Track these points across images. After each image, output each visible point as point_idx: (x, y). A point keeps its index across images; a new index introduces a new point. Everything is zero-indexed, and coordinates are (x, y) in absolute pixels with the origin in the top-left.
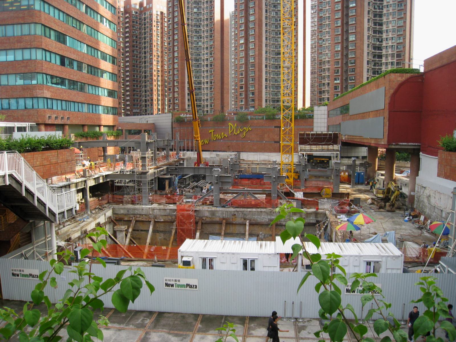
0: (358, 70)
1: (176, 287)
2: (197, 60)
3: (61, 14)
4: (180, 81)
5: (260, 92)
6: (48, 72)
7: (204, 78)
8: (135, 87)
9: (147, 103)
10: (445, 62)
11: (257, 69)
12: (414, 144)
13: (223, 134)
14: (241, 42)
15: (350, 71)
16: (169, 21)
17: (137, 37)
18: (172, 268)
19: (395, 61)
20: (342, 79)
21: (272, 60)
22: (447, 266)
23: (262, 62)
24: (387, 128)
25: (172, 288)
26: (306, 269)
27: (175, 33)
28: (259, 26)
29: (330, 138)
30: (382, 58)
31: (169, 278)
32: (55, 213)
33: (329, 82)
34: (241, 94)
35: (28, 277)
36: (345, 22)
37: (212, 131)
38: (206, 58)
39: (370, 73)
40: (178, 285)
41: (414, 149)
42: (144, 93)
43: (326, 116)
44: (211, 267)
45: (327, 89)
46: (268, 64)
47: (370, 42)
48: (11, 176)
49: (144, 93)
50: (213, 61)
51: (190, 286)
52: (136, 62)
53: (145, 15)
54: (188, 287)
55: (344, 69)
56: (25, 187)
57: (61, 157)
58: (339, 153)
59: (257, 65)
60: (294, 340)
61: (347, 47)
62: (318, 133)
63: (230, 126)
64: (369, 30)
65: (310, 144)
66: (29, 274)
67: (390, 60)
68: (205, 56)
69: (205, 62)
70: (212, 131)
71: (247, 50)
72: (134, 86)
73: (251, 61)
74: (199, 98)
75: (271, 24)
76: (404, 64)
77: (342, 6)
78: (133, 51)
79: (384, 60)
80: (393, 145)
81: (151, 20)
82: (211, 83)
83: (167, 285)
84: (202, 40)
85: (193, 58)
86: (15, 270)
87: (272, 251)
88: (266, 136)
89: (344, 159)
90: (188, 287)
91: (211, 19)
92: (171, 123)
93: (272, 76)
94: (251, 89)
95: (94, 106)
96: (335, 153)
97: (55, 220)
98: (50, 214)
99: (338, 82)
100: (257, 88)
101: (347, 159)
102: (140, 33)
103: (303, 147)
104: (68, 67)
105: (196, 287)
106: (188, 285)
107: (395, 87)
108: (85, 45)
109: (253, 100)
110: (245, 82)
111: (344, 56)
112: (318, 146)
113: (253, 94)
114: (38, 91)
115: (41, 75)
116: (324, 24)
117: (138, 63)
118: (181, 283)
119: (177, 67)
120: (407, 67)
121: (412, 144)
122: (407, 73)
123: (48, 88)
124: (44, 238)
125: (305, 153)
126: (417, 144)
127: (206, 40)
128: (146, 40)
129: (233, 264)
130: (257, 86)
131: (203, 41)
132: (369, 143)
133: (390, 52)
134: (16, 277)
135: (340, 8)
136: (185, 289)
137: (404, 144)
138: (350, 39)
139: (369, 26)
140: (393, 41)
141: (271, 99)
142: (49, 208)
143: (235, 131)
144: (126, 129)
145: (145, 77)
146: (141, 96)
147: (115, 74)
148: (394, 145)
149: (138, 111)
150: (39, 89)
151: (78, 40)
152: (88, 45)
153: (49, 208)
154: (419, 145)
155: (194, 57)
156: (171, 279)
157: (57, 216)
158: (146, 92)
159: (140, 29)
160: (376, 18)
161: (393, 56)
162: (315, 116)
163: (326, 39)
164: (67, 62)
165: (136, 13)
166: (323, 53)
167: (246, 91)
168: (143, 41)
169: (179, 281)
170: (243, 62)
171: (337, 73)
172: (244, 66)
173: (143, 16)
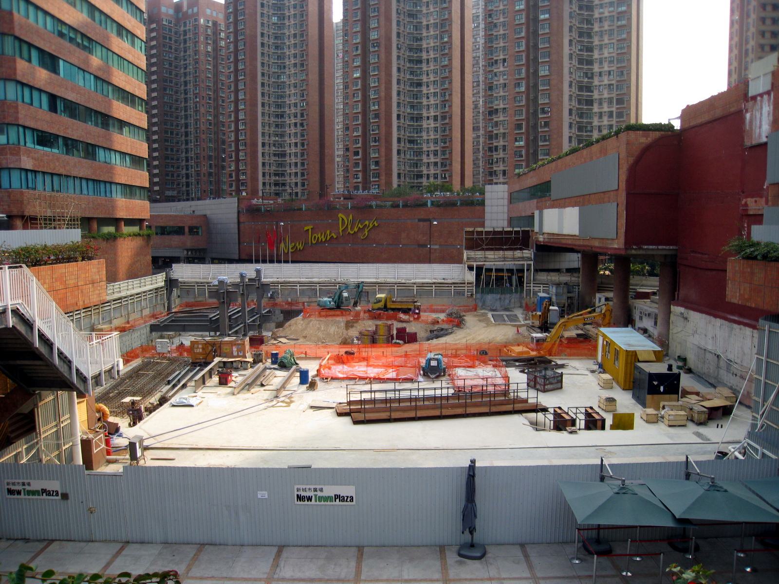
1: (316, 501)
2: (279, 106)
3: (49, 19)
4: (248, 141)
5: (389, 161)
6: (27, 124)
7: (290, 137)
8: (169, 153)
10: (719, 113)
11: (383, 122)
13: (328, 232)
14: (355, 75)
15: (541, 126)
16: (228, 38)
17: (170, 65)
19: (614, 109)
20: (527, 139)
22: (761, 446)
23: (391, 110)
24: (623, 221)
25: (309, 503)
28: (386, 48)
29: (517, 239)
30: (592, 105)
31: (304, 487)
32: (85, 377)
33: (506, 144)
34: (357, 165)
35: (39, 495)
36: (531, 44)
37: (310, 227)
38: (293, 102)
39: (573, 129)
40: (319, 497)
41: (665, 256)
42: (184, 163)
43: (506, 202)
45: (501, 155)
46: (401, 113)
47: (574, 77)
48: (16, 312)
49: (184, 162)
51: (342, 499)
52: (170, 108)
53: (185, 26)
54: (337, 500)
55: (531, 123)
56: (38, 330)
57: (83, 276)
58: (532, 263)
59: (382, 115)
60: (531, 581)
61: (536, 86)
62: (496, 230)
63: (341, 219)
64: (571, 58)
65: (483, 249)
66: (40, 489)
67: (606, 108)
68: (292, 98)
69: (292, 108)
70: (310, 227)
72: (167, 149)
73: (372, 108)
76: (629, 115)
77: (527, 18)
78: (165, 89)
79: (596, 108)
81: (196, 34)
82: (303, 145)
83: (300, 498)
86: (14, 484)
88: (404, 235)
89: (539, 273)
90: (337, 500)
91: (302, 35)
92: (236, 215)
94: (373, 155)
95: (108, 185)
96: (525, 263)
100: (383, 154)
101: (545, 274)
102: (176, 58)
103: (472, 253)
104: (63, 114)
106: (337, 497)
108: (92, 77)
109: (378, 175)
110: (362, 144)
111: (531, 101)
112: (497, 252)
113: (377, 163)
114: (8, 156)
115: (15, 128)
116: (497, 48)
117: (173, 110)
118: (325, 493)
119: (243, 117)
120: (633, 121)
121: (664, 247)
123: (29, 152)
124: (54, 424)
125: (475, 264)
126: (671, 247)
127: (293, 72)
128: (188, 70)
130: (383, 150)
131: (288, 73)
132: (588, 246)
133: (606, 95)
134: (16, 496)
135: (523, 21)
136: (331, 503)
137: (651, 247)
138: (541, 73)
139: (572, 52)
140: (611, 77)
143: (349, 227)
144: (158, 224)
145: (187, 134)
146: (178, 168)
148: (635, 249)
149: (175, 193)
150: (12, 154)
151: (79, 68)
152: (96, 77)
154: (675, 249)
156: (308, 487)
158: (187, 161)
159: (176, 51)
160: (582, 39)
161: (610, 101)
162: (487, 202)
163: (500, 72)
164: (60, 106)
165: (170, 22)
166: (495, 95)
168: (182, 71)
169: (321, 490)
170: (359, 110)
173: (182, 29)
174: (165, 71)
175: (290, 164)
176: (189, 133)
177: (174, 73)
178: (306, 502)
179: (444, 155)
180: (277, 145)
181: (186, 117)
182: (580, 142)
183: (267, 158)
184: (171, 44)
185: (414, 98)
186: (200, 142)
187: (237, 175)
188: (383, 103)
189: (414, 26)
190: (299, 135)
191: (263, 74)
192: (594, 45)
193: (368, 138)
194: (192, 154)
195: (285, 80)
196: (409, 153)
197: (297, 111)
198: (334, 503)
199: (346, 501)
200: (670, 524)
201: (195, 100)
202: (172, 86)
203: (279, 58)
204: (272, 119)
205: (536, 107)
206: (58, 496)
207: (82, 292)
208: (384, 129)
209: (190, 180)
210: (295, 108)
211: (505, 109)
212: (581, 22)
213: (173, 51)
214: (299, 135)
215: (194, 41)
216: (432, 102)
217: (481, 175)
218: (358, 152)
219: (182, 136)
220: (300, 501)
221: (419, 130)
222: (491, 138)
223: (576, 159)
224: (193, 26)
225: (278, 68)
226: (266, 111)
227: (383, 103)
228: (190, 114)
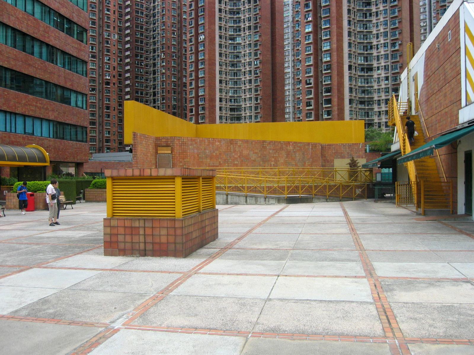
4: (207, 97)
11: (335, 73)
14: (307, 31)
17: (142, 35)
21: (359, 15)
23: (343, 60)
27: (200, 49)
34: (308, 104)
46: (352, 64)
50: (259, 65)
68: (247, 76)
71: (317, 43)
72: (137, 92)
73: (324, 60)
74: (237, 115)
75: (356, 32)
84: (242, 33)
85: (228, 62)
93: (360, 84)
145: (155, 95)
155: (229, 77)
172: (312, 68)
174: (137, 63)
175: (245, 117)
176: (157, 93)
177: (144, 56)
180: (233, 101)
183: (224, 112)
184: (143, 10)
185: (364, 49)
188: (335, 54)
189: (364, 57)
190: (253, 91)
191: (220, 37)
193: (320, 89)
194: (159, 45)
195: (240, 42)
196: (359, 36)
201: (162, 64)
203: (235, 74)
204: (229, 77)
208: (336, 79)
213: (144, 16)
214: (253, 91)
215: (162, 36)
216: (383, 53)
219: (150, 96)
224: (161, 8)
225: (234, 32)
226: (223, 70)
227: (335, 54)
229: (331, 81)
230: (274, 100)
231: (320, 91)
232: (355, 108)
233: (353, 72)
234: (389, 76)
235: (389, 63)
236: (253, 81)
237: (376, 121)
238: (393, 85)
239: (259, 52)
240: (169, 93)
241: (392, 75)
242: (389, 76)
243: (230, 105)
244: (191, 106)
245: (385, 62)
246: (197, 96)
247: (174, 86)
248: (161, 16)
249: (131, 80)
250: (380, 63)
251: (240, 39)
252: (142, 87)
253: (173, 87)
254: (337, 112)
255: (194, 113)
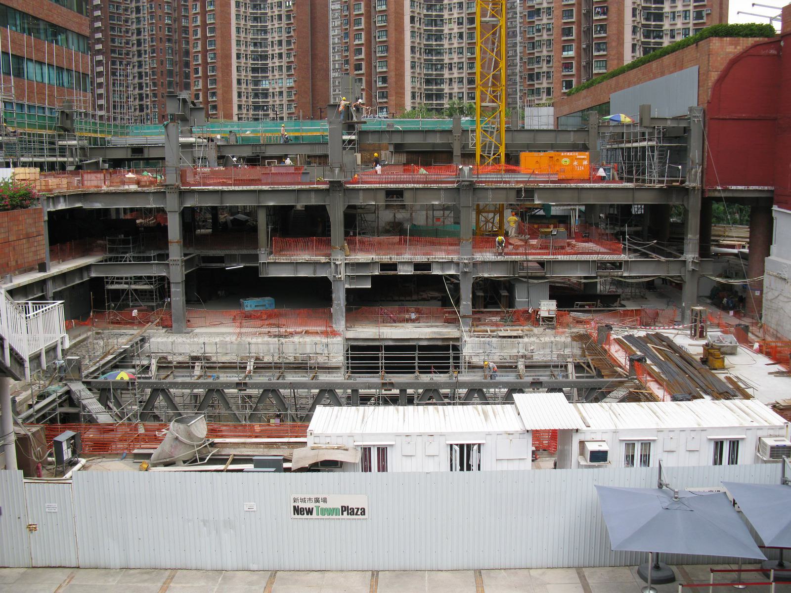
0: (612, 29)
5: (400, 76)
9: (144, 102)
12: (761, 188)
18: (342, 473)
20: (579, 48)
23: (403, 10)
25: (309, 516)
26: (591, 460)
32: (22, 359)
44: (382, 467)
50: (292, 8)
54: (345, 513)
55: (584, 26)
73: (379, 8)
80: (716, 190)
83: (297, 510)
87: (517, 427)
90: (345, 513)
97: (24, 375)
98: (13, 361)
99: (571, 54)
100: (392, 67)
105: (363, 512)
106: (345, 509)
107: (722, 67)
109: (384, 95)
110: (366, 55)
113: (384, 80)
117: (121, 11)
121: (756, 188)
122: (746, 36)
126: (766, 188)
129: (691, 454)
130: (392, 62)
136: (337, 517)
137: (740, 188)
141: (423, 91)
142: (10, 346)
147: (84, 37)
153: (10, 346)
156: (307, 496)
157: (27, 364)
167: (369, 74)
171: (567, 35)
175: (273, 67)
178: (305, 516)
179: (471, 68)
181: (139, 43)
182: (646, 51)
183: (243, 73)
186: (155, 9)
187: (206, 97)
192: (664, 11)
195: (268, 86)
197: (282, 51)
198: (341, 517)
199: (356, 514)
200: (760, 555)
202: (121, 25)
204: (250, 23)
205: (589, 41)
206: (364, 514)
207: (14, 248)
209: (142, 37)
210: (279, 9)
211: (550, 8)
212: (647, 36)
217: (519, 94)
218: (360, 65)
220: (298, 514)
221: (439, 66)
222: (531, 77)
223: (643, 75)
226: (243, 103)
228: (144, 39)
229: (386, 37)
230: (314, 57)
231: (373, 50)
232: (419, 74)
233: (417, 25)
234: (463, 32)
235: (463, 15)
236: (284, 56)
237: (446, 91)
238: (469, 44)
239: (293, 53)
240: (161, 42)
241: (467, 30)
242: (463, 32)
243: (251, 39)
244: (197, 90)
245: (459, 13)
246: (204, 24)
247: (169, 32)
248: (148, 13)
249: (103, 20)
250: (453, 14)
251: (267, 82)
252: (121, 43)
253: (167, 33)
254: (394, 79)
255: (200, 74)
